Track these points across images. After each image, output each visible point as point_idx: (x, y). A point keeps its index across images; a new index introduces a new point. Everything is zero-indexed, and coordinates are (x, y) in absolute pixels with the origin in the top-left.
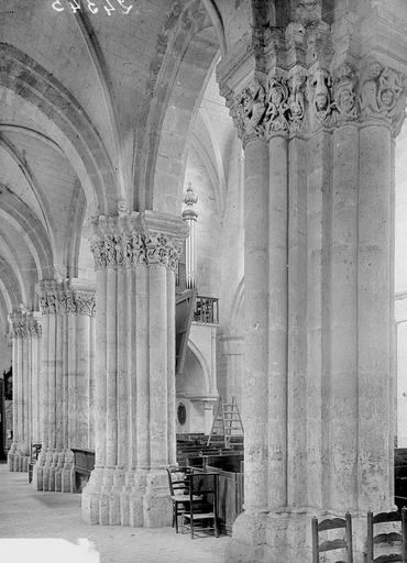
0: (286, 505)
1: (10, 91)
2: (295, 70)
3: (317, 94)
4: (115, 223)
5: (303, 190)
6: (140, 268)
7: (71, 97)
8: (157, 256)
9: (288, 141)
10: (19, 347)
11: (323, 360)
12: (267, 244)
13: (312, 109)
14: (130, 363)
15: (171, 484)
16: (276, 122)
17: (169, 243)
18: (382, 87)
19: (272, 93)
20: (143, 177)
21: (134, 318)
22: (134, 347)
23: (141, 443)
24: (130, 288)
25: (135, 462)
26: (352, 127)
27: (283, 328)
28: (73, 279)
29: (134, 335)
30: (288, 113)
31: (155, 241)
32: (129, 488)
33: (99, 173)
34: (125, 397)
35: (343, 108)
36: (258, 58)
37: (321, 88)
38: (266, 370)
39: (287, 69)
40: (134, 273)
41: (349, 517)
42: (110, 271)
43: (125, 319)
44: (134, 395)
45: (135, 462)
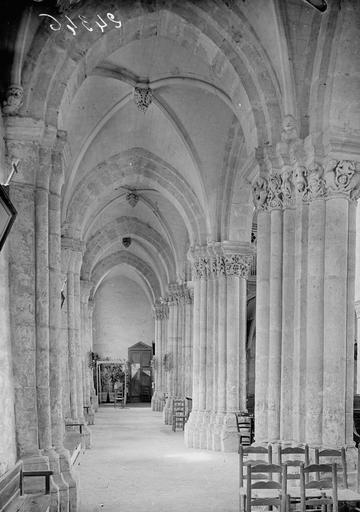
0: (279, 438)
1: (141, 176)
2: (284, 169)
3: (298, 180)
4: (205, 250)
5: (292, 241)
6: (221, 279)
7: (178, 173)
8: (232, 270)
9: (283, 211)
10: (176, 313)
11: (301, 349)
12: (269, 275)
13: (296, 191)
14: (214, 342)
15: (238, 424)
16: (274, 202)
17: (241, 261)
18: (338, 174)
19: (270, 185)
20: (223, 218)
21: (217, 312)
22: (217, 331)
23: (221, 396)
24: (215, 291)
25: (216, 408)
26: (320, 200)
27: (277, 329)
28: (188, 282)
29: (217, 323)
30: (281, 197)
31: (230, 260)
32: (212, 425)
33: (196, 219)
34: (211, 364)
35: (314, 189)
36: (261, 165)
37: (300, 179)
38: (268, 355)
39: (280, 168)
40: (217, 282)
41: (344, 450)
42: (203, 281)
43: (212, 312)
44: (217, 363)
45: (216, 408)
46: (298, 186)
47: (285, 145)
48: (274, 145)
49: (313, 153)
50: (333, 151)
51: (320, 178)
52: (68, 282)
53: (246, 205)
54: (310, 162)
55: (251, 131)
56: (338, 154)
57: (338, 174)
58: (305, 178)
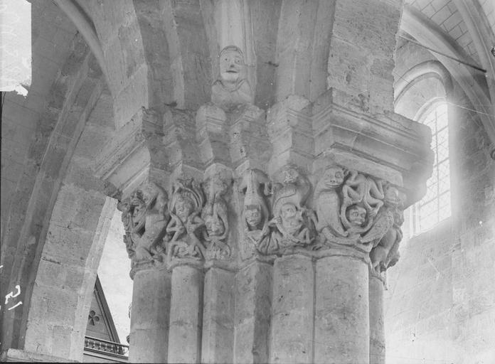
2: (212, 170)
16: (181, 245)
18: (347, 200)
36: (153, 150)
37: (252, 198)
39: (202, 166)
46: (251, 216)
47: (220, 115)
48: (191, 110)
49: (289, 143)
50: (336, 146)
51: (303, 204)
52: (54, 262)
53: (79, 269)
54: (282, 155)
55: (130, 71)
56: (349, 156)
57: (347, 200)
58: (265, 198)
